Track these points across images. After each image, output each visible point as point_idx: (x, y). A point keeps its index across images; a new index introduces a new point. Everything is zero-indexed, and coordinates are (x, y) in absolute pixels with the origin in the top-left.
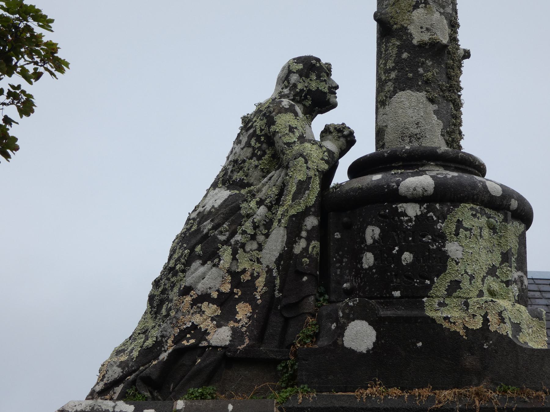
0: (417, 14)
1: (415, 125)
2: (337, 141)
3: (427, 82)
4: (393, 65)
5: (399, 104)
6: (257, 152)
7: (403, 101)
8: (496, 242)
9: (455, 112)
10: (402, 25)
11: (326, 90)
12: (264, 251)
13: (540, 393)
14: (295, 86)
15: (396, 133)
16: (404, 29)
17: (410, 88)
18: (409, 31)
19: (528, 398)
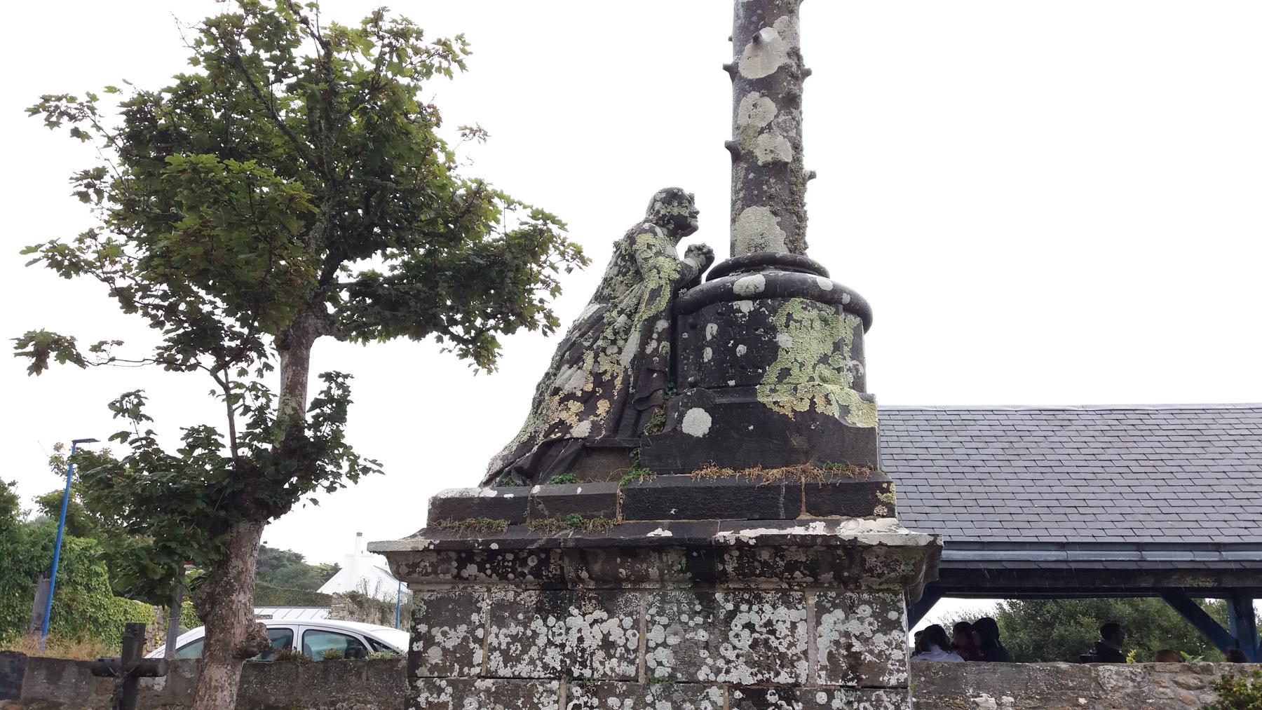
3: (771, 197)
8: (828, 333)
9: (798, 223)
11: (687, 214)
12: (623, 353)
13: (864, 469)
14: (658, 212)
16: (750, 153)
17: (756, 204)
19: (853, 473)
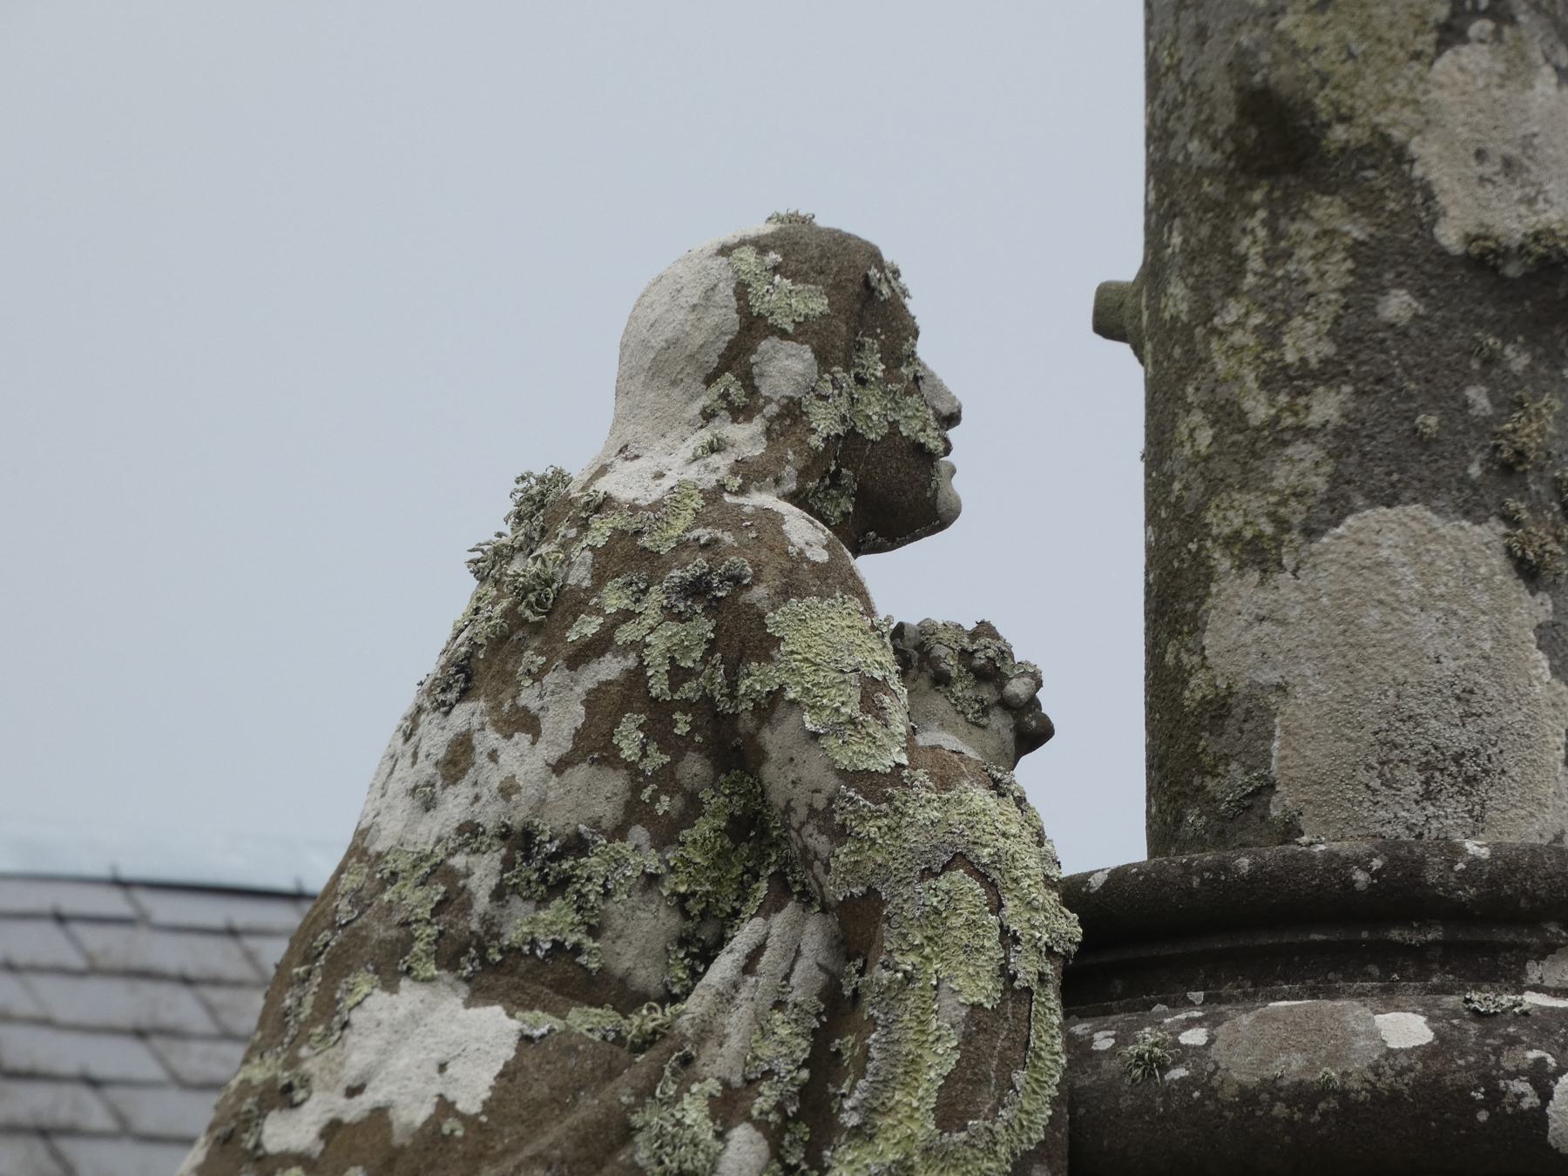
0: (1459, 76)
1: (1453, 702)
2: (977, 732)
4: (1328, 349)
5: (1365, 580)
6: (655, 798)
7: (1387, 563)
10: (1380, 129)
14: (793, 413)
15: (1350, 740)
18: (1418, 171)
